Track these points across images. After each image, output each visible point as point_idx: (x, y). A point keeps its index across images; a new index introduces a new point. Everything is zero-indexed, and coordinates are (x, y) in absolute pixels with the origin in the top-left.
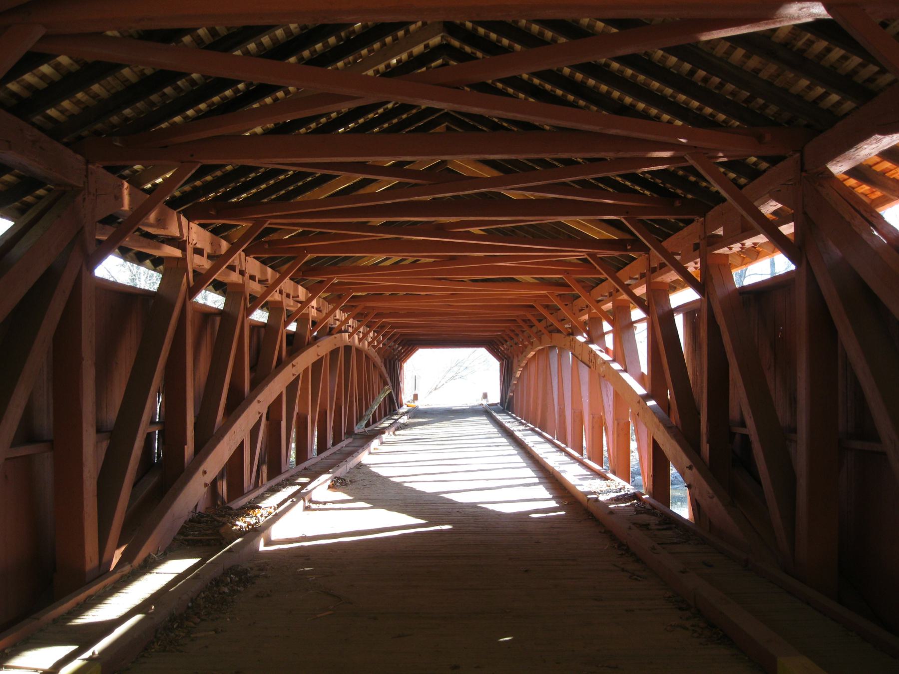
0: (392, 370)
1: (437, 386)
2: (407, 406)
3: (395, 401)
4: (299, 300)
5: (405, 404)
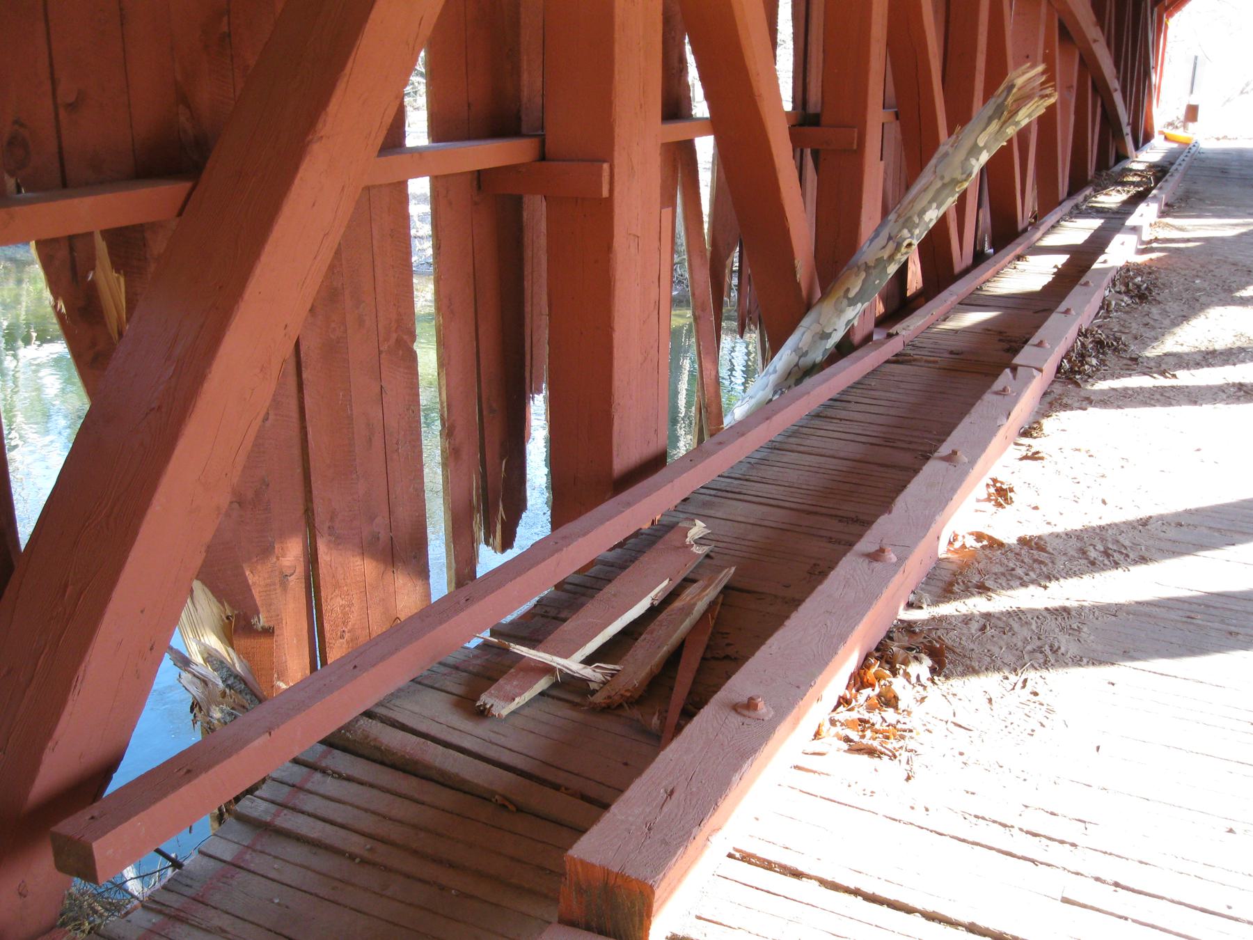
0: (1128, 22)
1: (1247, 85)
2: (1166, 138)
3: (1127, 130)
4: (187, 792)
5: (1161, 133)
